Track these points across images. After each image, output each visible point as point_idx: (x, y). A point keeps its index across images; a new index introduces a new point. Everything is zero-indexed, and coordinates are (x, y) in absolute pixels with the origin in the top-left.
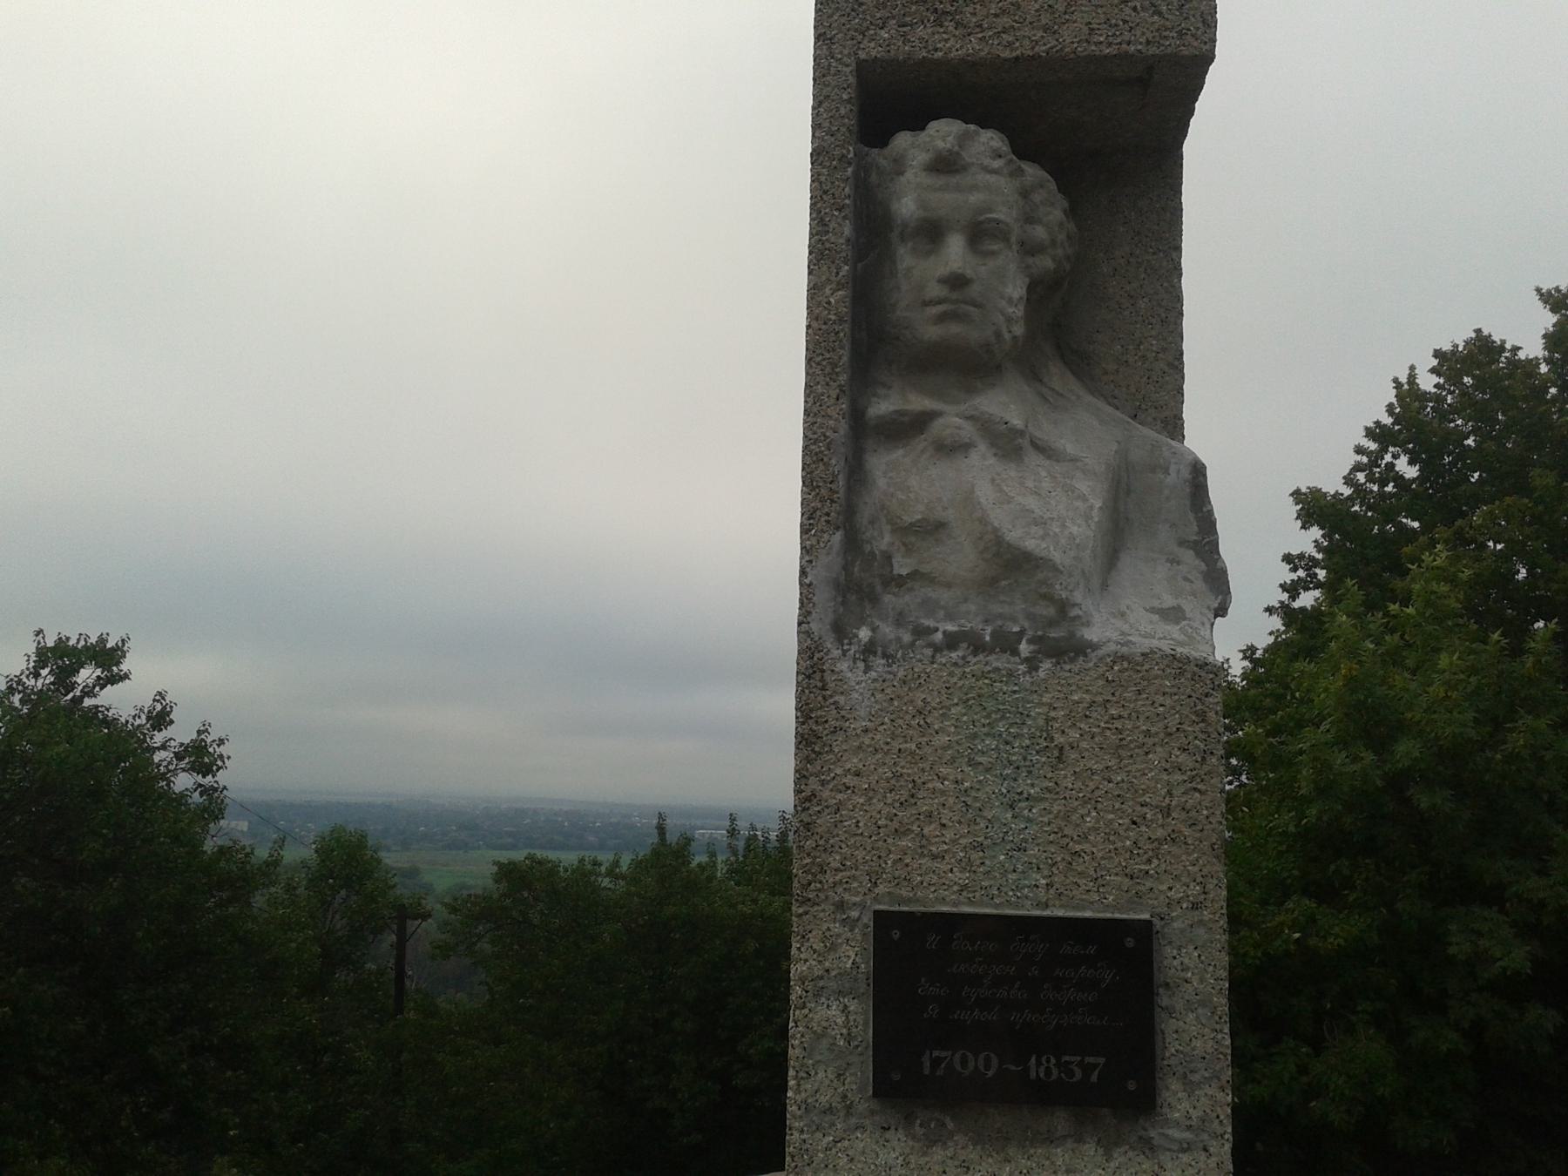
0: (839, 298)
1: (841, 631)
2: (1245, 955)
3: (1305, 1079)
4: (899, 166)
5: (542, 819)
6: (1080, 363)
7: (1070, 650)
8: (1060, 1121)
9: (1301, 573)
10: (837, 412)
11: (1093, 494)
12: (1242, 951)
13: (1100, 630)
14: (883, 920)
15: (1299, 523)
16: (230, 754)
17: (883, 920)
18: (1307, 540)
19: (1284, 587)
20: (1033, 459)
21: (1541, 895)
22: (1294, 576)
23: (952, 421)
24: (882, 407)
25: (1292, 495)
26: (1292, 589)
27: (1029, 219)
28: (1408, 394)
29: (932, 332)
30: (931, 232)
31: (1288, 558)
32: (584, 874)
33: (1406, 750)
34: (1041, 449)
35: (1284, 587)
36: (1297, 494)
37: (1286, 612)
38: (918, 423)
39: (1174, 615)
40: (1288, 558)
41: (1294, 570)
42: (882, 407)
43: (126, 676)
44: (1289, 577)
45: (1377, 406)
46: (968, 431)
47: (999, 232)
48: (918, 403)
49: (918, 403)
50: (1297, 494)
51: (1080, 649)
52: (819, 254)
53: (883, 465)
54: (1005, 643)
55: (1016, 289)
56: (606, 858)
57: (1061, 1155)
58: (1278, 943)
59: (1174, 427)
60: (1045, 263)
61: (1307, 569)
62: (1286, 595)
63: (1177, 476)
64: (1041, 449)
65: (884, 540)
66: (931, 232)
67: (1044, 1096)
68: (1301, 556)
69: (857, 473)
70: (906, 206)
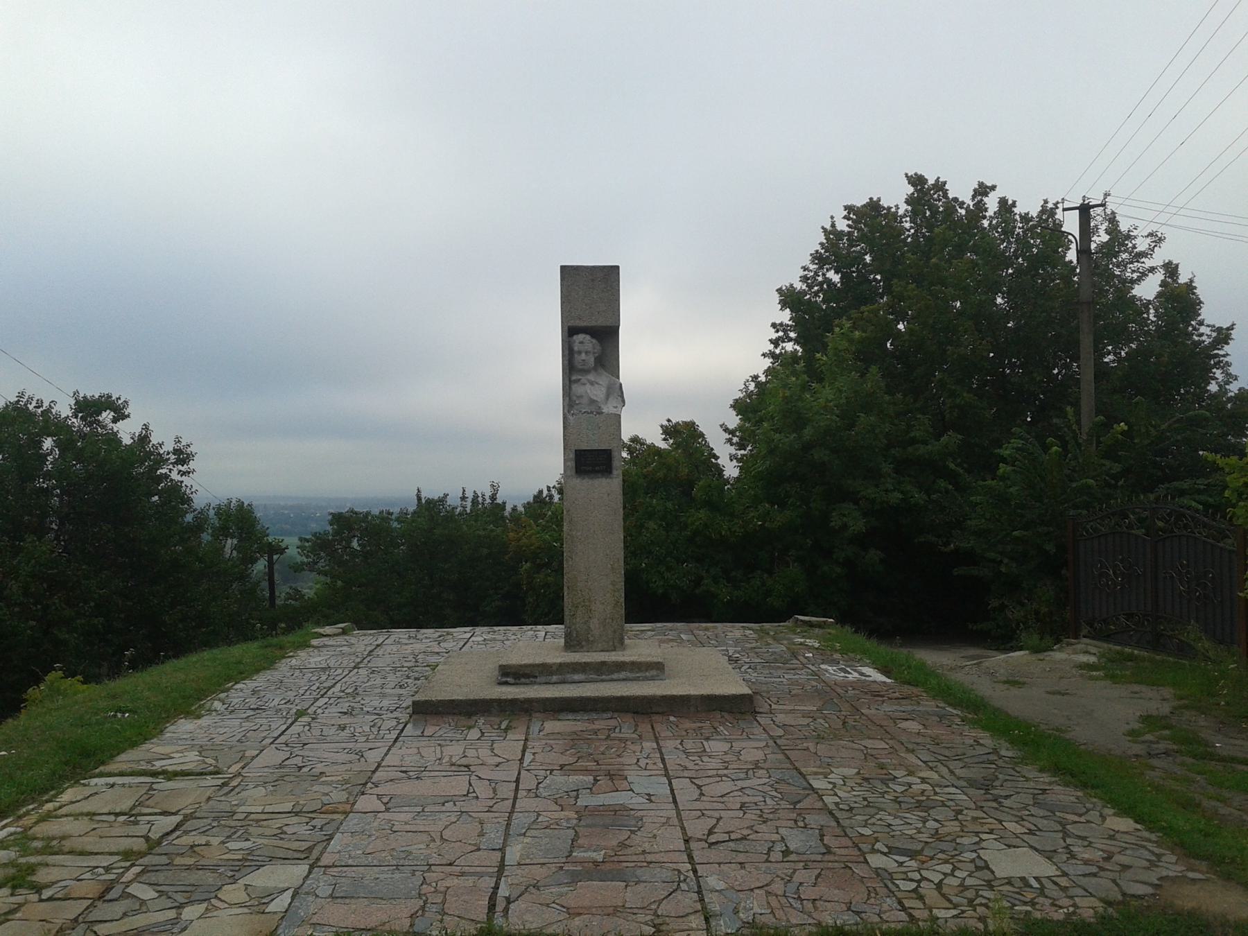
0: (566, 362)
1: (569, 412)
2: (735, 531)
3: (764, 588)
4: (575, 342)
5: (272, 512)
6: (603, 366)
7: (600, 413)
8: (600, 475)
9: (781, 334)
10: (567, 380)
11: (604, 390)
12: (733, 530)
13: (605, 410)
14: (576, 451)
15: (780, 306)
16: (667, 418)
17: (576, 451)
18: (785, 317)
19: (771, 341)
20: (596, 385)
21: (873, 496)
22: (777, 335)
23: (584, 380)
24: (574, 378)
25: (777, 290)
26: (775, 342)
27: (594, 349)
28: (832, 234)
29: (580, 367)
30: (580, 353)
31: (774, 325)
32: (385, 517)
33: (808, 432)
34: (597, 383)
35: (771, 341)
36: (779, 291)
37: (772, 355)
38: (579, 380)
39: (616, 407)
40: (774, 325)
41: (777, 331)
42: (574, 378)
43: (128, 416)
44: (774, 336)
45: (815, 241)
46: (586, 382)
47: (590, 352)
48: (580, 377)
49: (580, 377)
50: (779, 291)
51: (602, 413)
52: (563, 356)
53: (574, 387)
54: (592, 412)
55: (593, 360)
56: (396, 510)
57: (600, 480)
58: (751, 526)
59: (618, 378)
60: (597, 355)
61: (785, 331)
62: (773, 346)
63: (618, 385)
64: (597, 383)
65: (575, 398)
66: (580, 353)
67: (598, 472)
68: (781, 324)
69: (570, 387)
70: (576, 349)
